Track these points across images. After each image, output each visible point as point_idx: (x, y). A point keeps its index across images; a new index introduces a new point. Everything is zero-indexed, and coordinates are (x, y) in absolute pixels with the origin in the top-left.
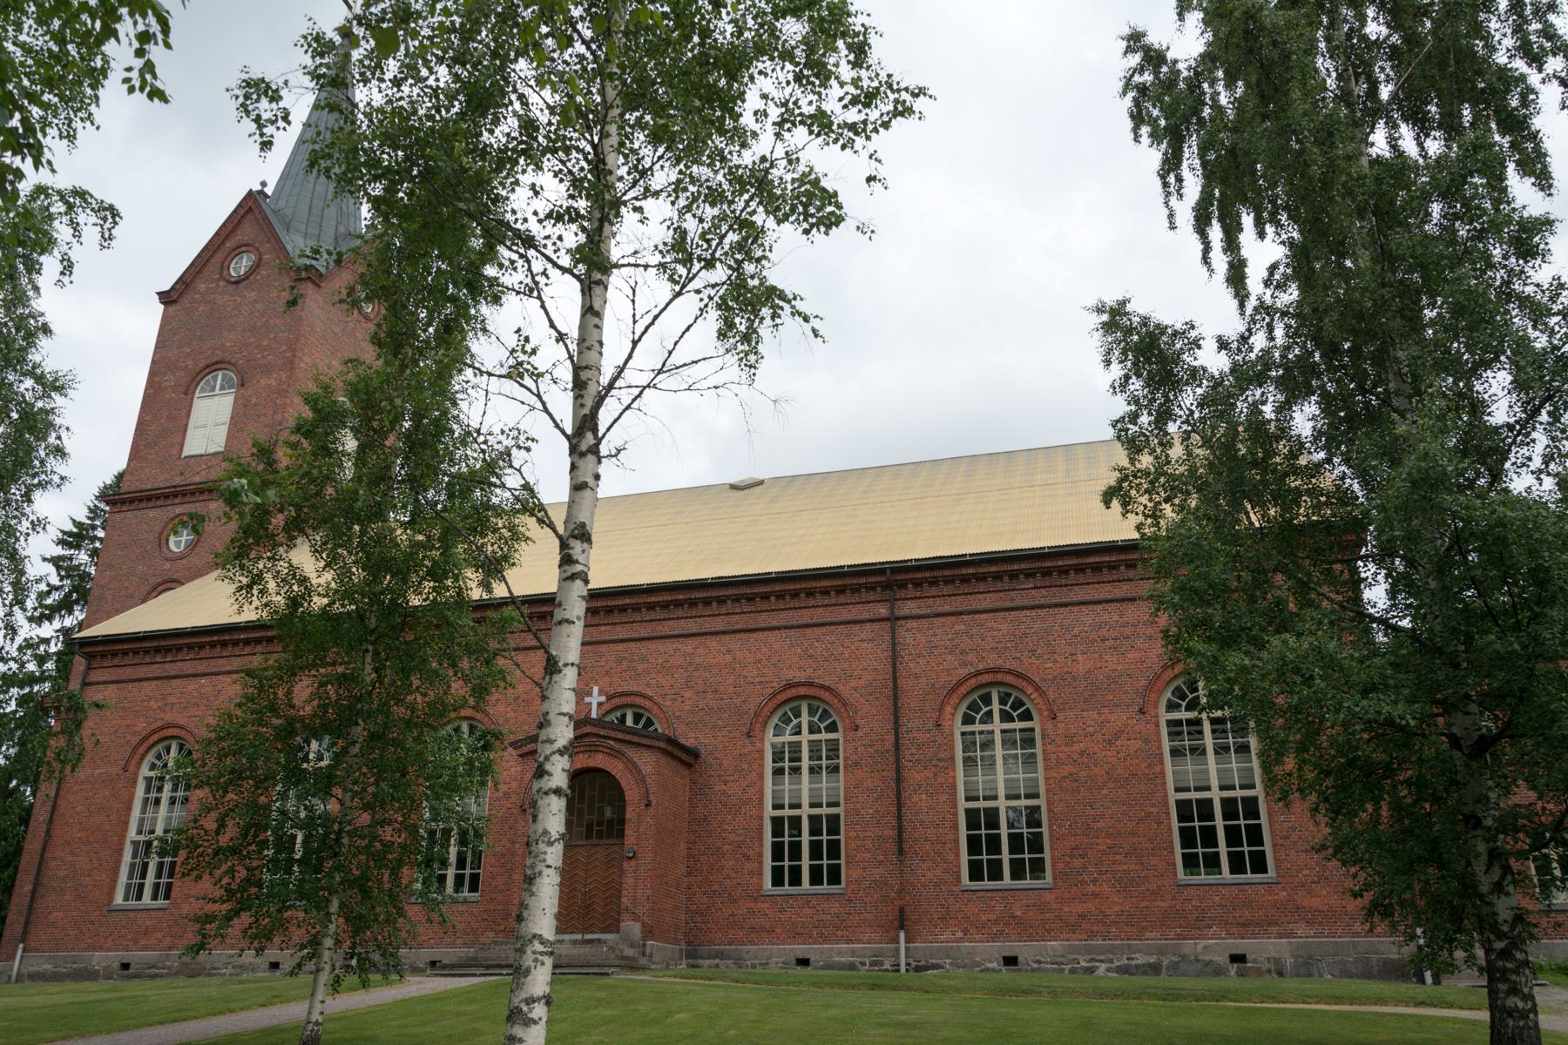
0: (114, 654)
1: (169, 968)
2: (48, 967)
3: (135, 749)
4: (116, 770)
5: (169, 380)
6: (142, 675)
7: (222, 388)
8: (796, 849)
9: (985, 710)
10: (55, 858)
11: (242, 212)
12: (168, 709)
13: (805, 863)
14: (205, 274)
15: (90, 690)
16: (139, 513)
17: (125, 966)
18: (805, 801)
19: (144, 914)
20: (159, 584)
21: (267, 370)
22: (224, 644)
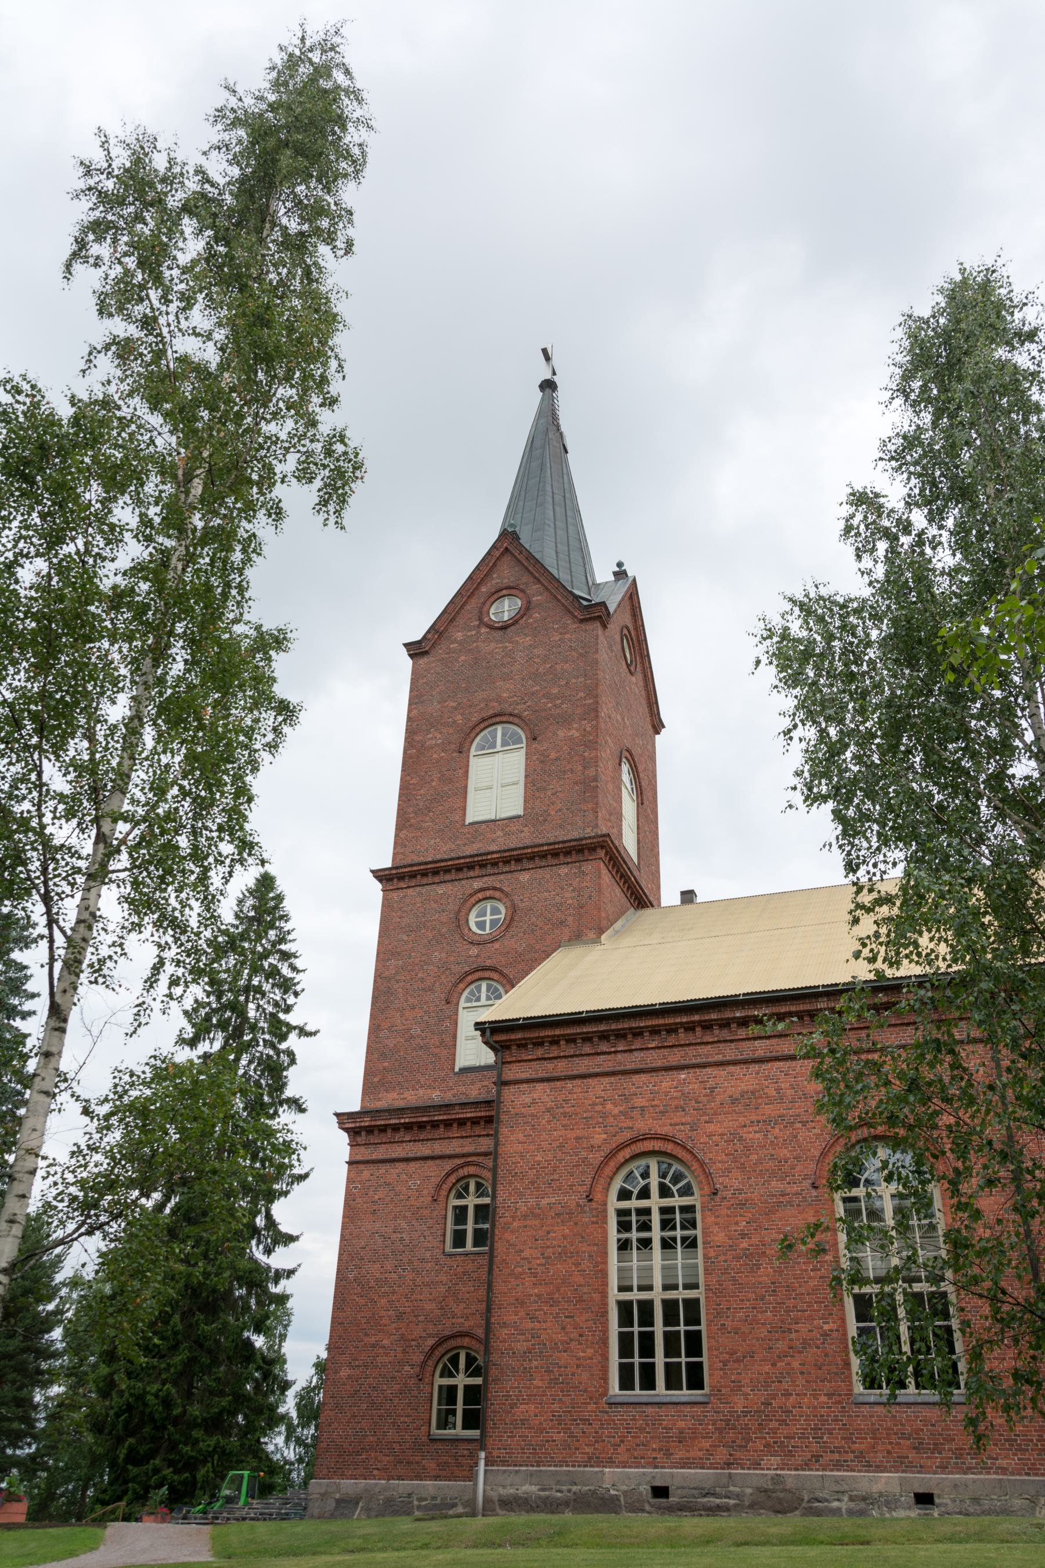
0: (539, 1043)
1: (738, 1496)
2: (529, 1489)
3: (600, 1168)
4: (573, 1200)
5: (435, 738)
6: (583, 1070)
7: (504, 743)
8: (647, 1340)
9: (674, 1189)
10: (505, 1325)
11: (497, 554)
12: (635, 1113)
13: (660, 1359)
14: (460, 621)
15: (508, 1092)
16: (424, 890)
17: (660, 1492)
18: (658, 1282)
19: (672, 1411)
20: (467, 974)
21: (565, 720)
22: (707, 1026)
